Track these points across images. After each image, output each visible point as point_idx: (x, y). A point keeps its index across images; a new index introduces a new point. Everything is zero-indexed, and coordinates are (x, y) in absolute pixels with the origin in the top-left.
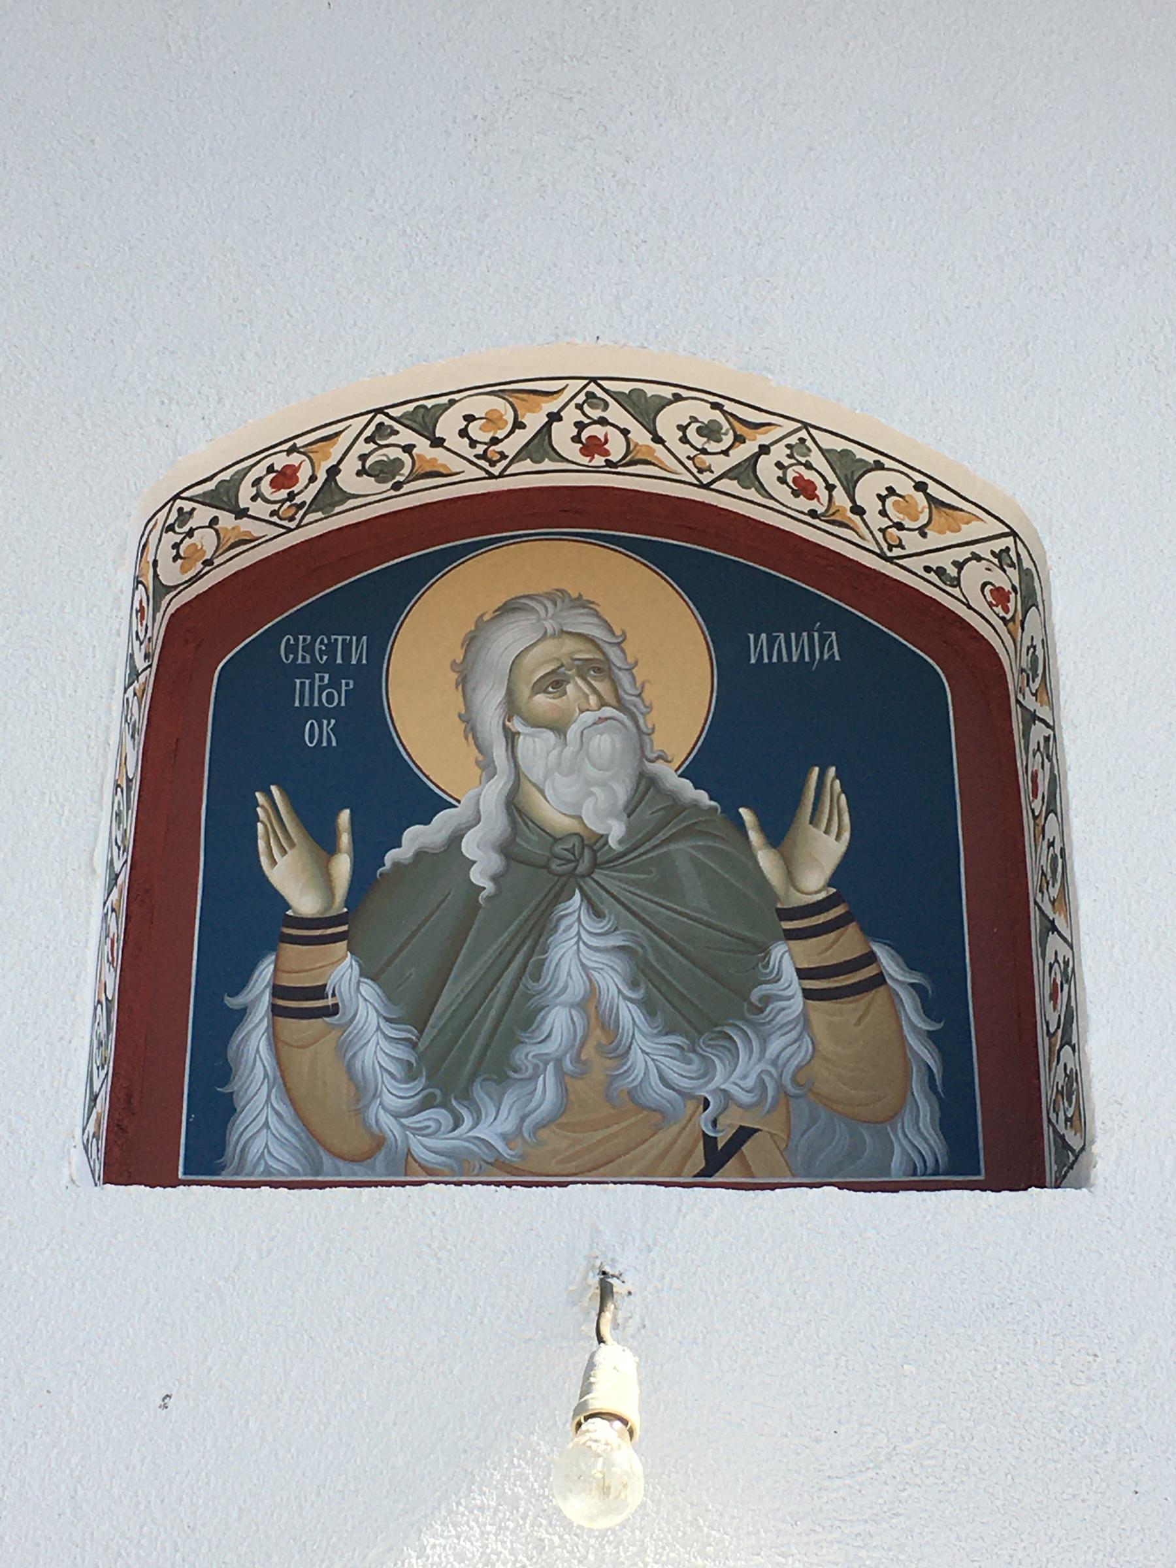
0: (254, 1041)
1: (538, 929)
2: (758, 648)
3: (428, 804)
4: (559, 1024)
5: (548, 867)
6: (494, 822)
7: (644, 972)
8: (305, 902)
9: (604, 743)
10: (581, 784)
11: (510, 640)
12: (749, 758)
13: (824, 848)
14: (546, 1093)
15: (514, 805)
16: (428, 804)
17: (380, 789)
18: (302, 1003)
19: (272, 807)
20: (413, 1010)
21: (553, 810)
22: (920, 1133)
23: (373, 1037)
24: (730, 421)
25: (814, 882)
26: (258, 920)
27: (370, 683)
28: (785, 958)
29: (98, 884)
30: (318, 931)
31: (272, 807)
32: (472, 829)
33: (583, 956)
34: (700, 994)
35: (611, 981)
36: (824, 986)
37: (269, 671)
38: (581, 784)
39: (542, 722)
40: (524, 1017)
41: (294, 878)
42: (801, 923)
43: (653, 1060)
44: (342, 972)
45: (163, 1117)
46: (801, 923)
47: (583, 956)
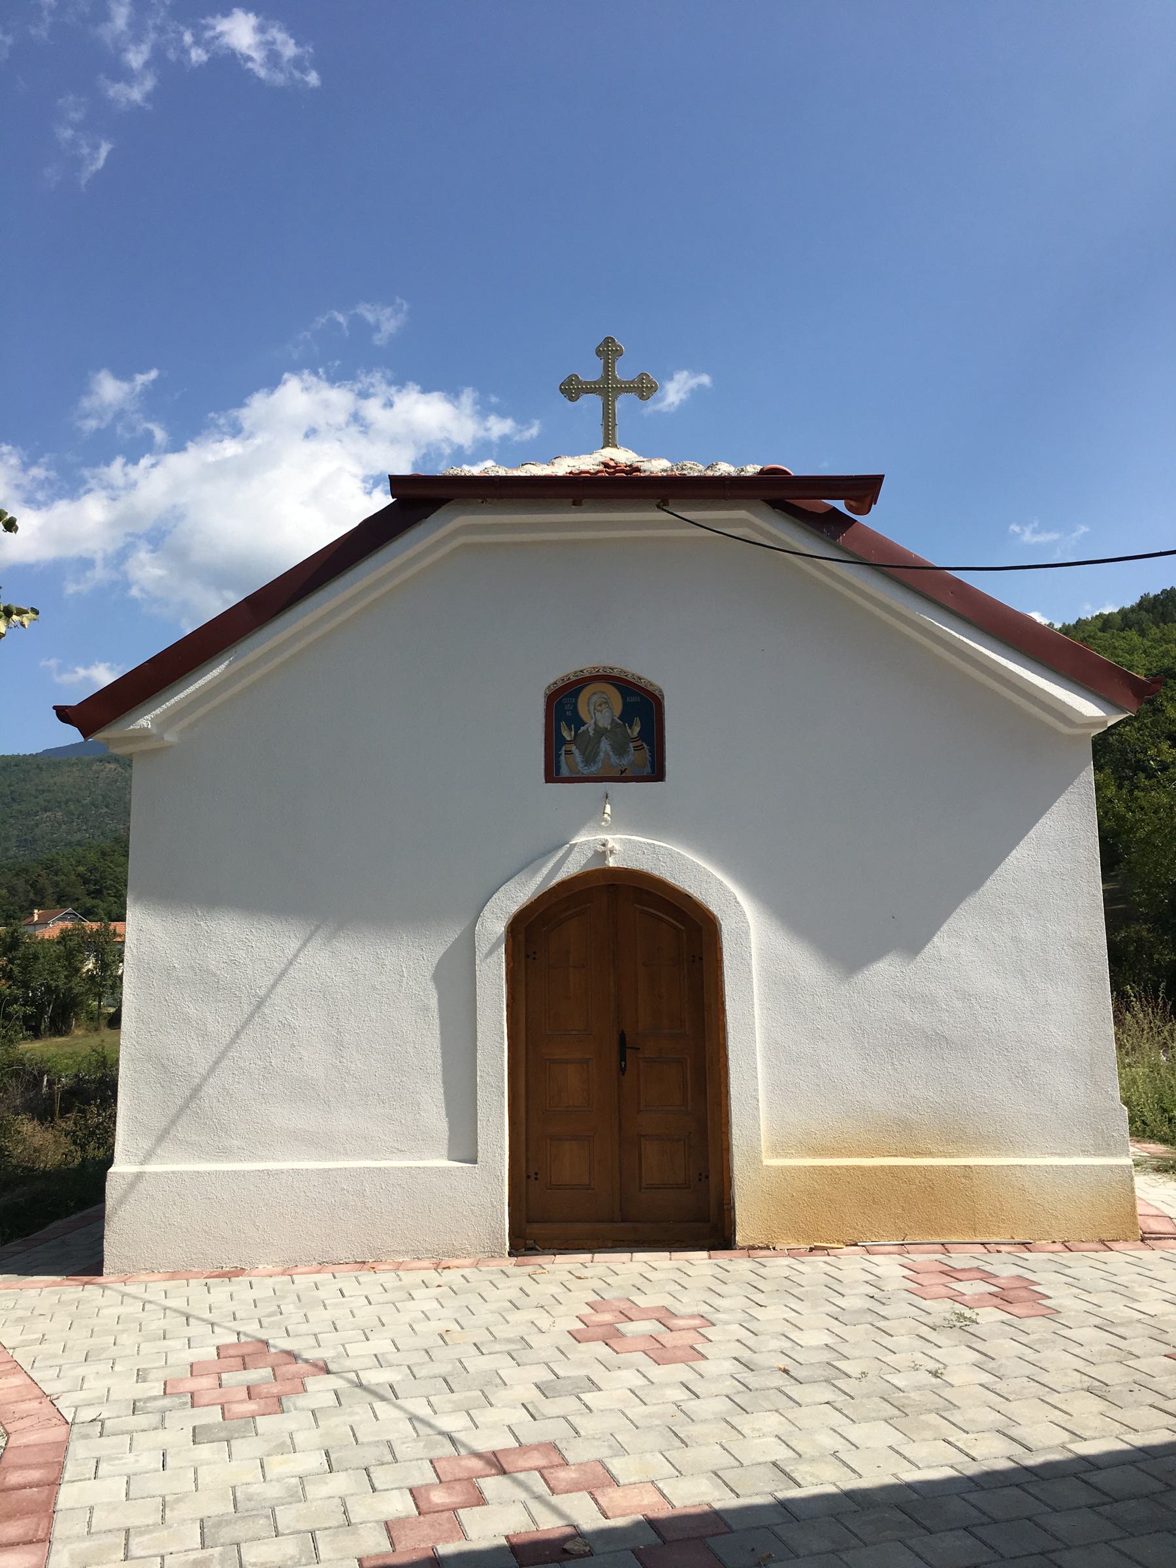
0: (563, 758)
1: (599, 742)
2: (628, 699)
3: (584, 724)
4: (602, 754)
5: (600, 732)
6: (593, 726)
7: (613, 747)
8: (568, 739)
9: (607, 714)
10: (604, 721)
11: (595, 698)
12: (627, 716)
13: (637, 729)
14: (600, 765)
15: (595, 724)
16: (584, 724)
17: (577, 722)
18: (568, 752)
19: (563, 724)
20: (583, 753)
21: (601, 724)
22: (1110, 824)
23: (578, 756)
24: (622, 671)
25: (635, 734)
26: (562, 741)
27: (575, 705)
28: (631, 745)
29: (489, 464)
30: (570, 742)
31: (563, 724)
32: (590, 727)
33: (605, 745)
34: (620, 751)
35: (609, 748)
36: (636, 748)
37: (562, 703)
38: (604, 721)
39: (599, 711)
40: (597, 754)
41: (567, 735)
42: (633, 740)
43: (614, 759)
44: (573, 748)
45: (552, 774)
46: (633, 740)
47: (605, 745)
